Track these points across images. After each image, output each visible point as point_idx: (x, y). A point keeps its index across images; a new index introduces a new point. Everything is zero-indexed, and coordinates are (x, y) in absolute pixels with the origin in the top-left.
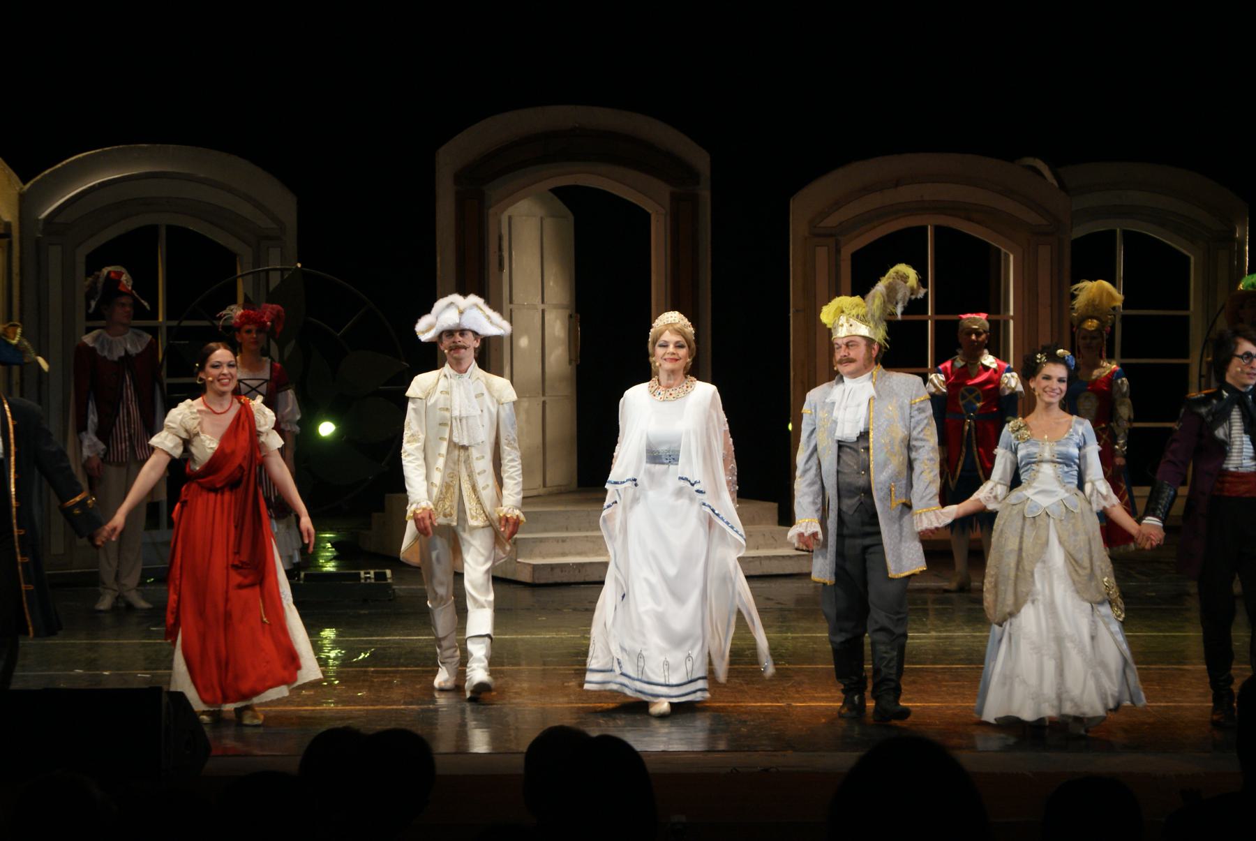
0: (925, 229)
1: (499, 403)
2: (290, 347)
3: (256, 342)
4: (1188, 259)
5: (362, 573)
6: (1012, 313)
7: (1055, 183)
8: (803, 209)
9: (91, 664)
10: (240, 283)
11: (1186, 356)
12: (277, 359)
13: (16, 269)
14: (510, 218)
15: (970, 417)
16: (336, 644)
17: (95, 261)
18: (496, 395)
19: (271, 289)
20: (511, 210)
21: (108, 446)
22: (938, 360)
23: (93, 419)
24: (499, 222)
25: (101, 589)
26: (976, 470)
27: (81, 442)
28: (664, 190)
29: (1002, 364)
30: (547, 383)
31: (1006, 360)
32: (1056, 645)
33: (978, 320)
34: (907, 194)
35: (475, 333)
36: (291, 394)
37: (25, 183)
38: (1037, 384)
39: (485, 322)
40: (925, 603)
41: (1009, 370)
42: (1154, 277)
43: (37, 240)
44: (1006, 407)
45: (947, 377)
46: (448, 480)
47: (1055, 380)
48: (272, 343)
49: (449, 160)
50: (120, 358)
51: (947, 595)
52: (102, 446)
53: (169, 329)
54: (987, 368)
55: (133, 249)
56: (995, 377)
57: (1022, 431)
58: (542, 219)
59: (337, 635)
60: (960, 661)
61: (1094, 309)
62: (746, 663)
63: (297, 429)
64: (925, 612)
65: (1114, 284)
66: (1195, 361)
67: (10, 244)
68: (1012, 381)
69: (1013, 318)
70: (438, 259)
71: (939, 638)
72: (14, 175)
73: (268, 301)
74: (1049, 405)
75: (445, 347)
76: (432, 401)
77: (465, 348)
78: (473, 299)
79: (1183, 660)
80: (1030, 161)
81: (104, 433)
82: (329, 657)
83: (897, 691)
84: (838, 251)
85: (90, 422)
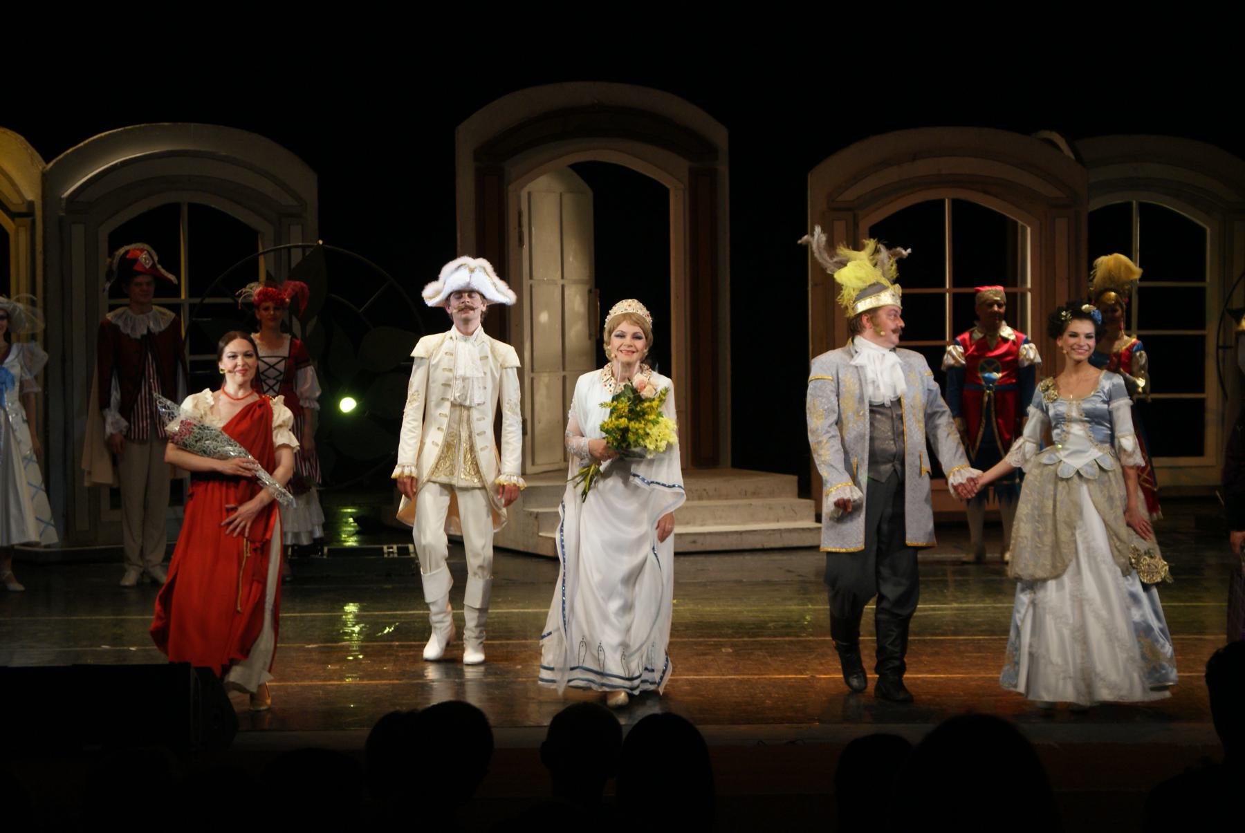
0: (942, 202)
1: (503, 367)
2: (313, 322)
3: (274, 319)
4: (1203, 231)
5: (385, 547)
6: (1029, 286)
7: (1072, 156)
8: (820, 183)
9: (116, 640)
10: (262, 260)
11: (1203, 327)
12: (299, 336)
13: (39, 248)
14: (529, 194)
15: (989, 388)
16: (359, 619)
17: (120, 237)
18: (500, 360)
19: (293, 266)
20: (531, 186)
21: (129, 421)
22: (956, 332)
23: (115, 396)
24: (519, 197)
25: (126, 566)
26: (995, 442)
27: (104, 420)
28: (683, 165)
29: (1020, 335)
30: (567, 358)
31: (1024, 330)
32: (1085, 615)
33: (994, 293)
34: (923, 167)
35: (483, 296)
36: (310, 371)
37: (47, 162)
38: (1065, 342)
39: (492, 289)
40: (945, 574)
41: (1027, 342)
42: (1171, 249)
43: (62, 218)
44: (1022, 382)
45: (966, 349)
46: (449, 439)
47: (1082, 337)
48: (295, 320)
49: (469, 135)
50: (143, 336)
51: (966, 567)
52: (124, 423)
53: (192, 306)
54: (1005, 340)
55: (156, 227)
56: (1015, 348)
57: (1051, 391)
58: (561, 195)
59: (361, 609)
60: (982, 632)
61: (1113, 282)
62: (769, 636)
63: (317, 406)
64: (945, 584)
65: (1130, 257)
66: (1211, 333)
67: (33, 222)
68: (1030, 352)
69: (1031, 290)
70: (458, 235)
71: (958, 609)
72: (36, 154)
73: (290, 278)
74: (1078, 362)
75: (452, 311)
76: (434, 362)
77: (473, 309)
78: (482, 262)
79: (1201, 630)
80: (1046, 134)
81: (126, 410)
82: (353, 632)
83: (902, 669)
84: (856, 225)
85: (113, 399)
